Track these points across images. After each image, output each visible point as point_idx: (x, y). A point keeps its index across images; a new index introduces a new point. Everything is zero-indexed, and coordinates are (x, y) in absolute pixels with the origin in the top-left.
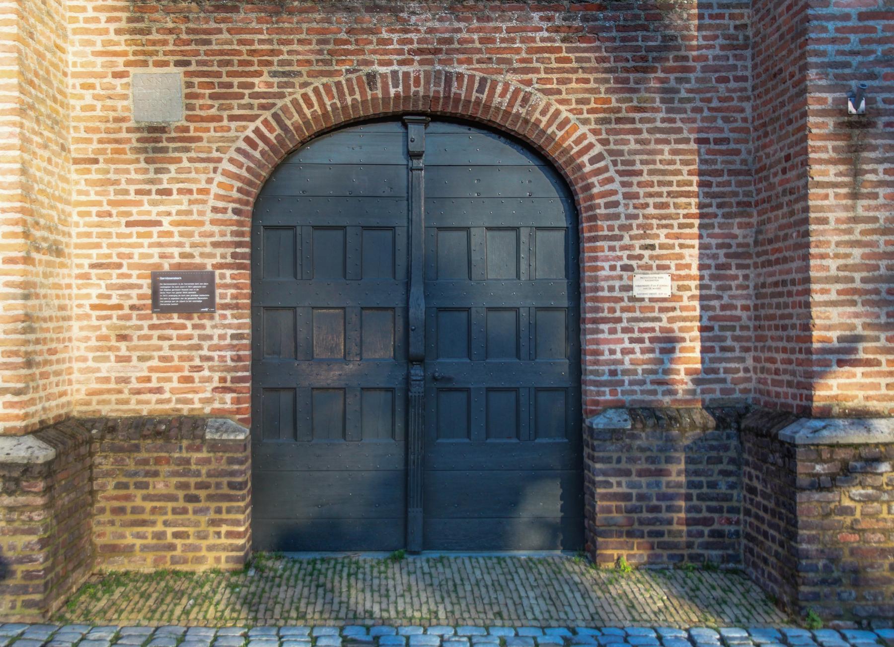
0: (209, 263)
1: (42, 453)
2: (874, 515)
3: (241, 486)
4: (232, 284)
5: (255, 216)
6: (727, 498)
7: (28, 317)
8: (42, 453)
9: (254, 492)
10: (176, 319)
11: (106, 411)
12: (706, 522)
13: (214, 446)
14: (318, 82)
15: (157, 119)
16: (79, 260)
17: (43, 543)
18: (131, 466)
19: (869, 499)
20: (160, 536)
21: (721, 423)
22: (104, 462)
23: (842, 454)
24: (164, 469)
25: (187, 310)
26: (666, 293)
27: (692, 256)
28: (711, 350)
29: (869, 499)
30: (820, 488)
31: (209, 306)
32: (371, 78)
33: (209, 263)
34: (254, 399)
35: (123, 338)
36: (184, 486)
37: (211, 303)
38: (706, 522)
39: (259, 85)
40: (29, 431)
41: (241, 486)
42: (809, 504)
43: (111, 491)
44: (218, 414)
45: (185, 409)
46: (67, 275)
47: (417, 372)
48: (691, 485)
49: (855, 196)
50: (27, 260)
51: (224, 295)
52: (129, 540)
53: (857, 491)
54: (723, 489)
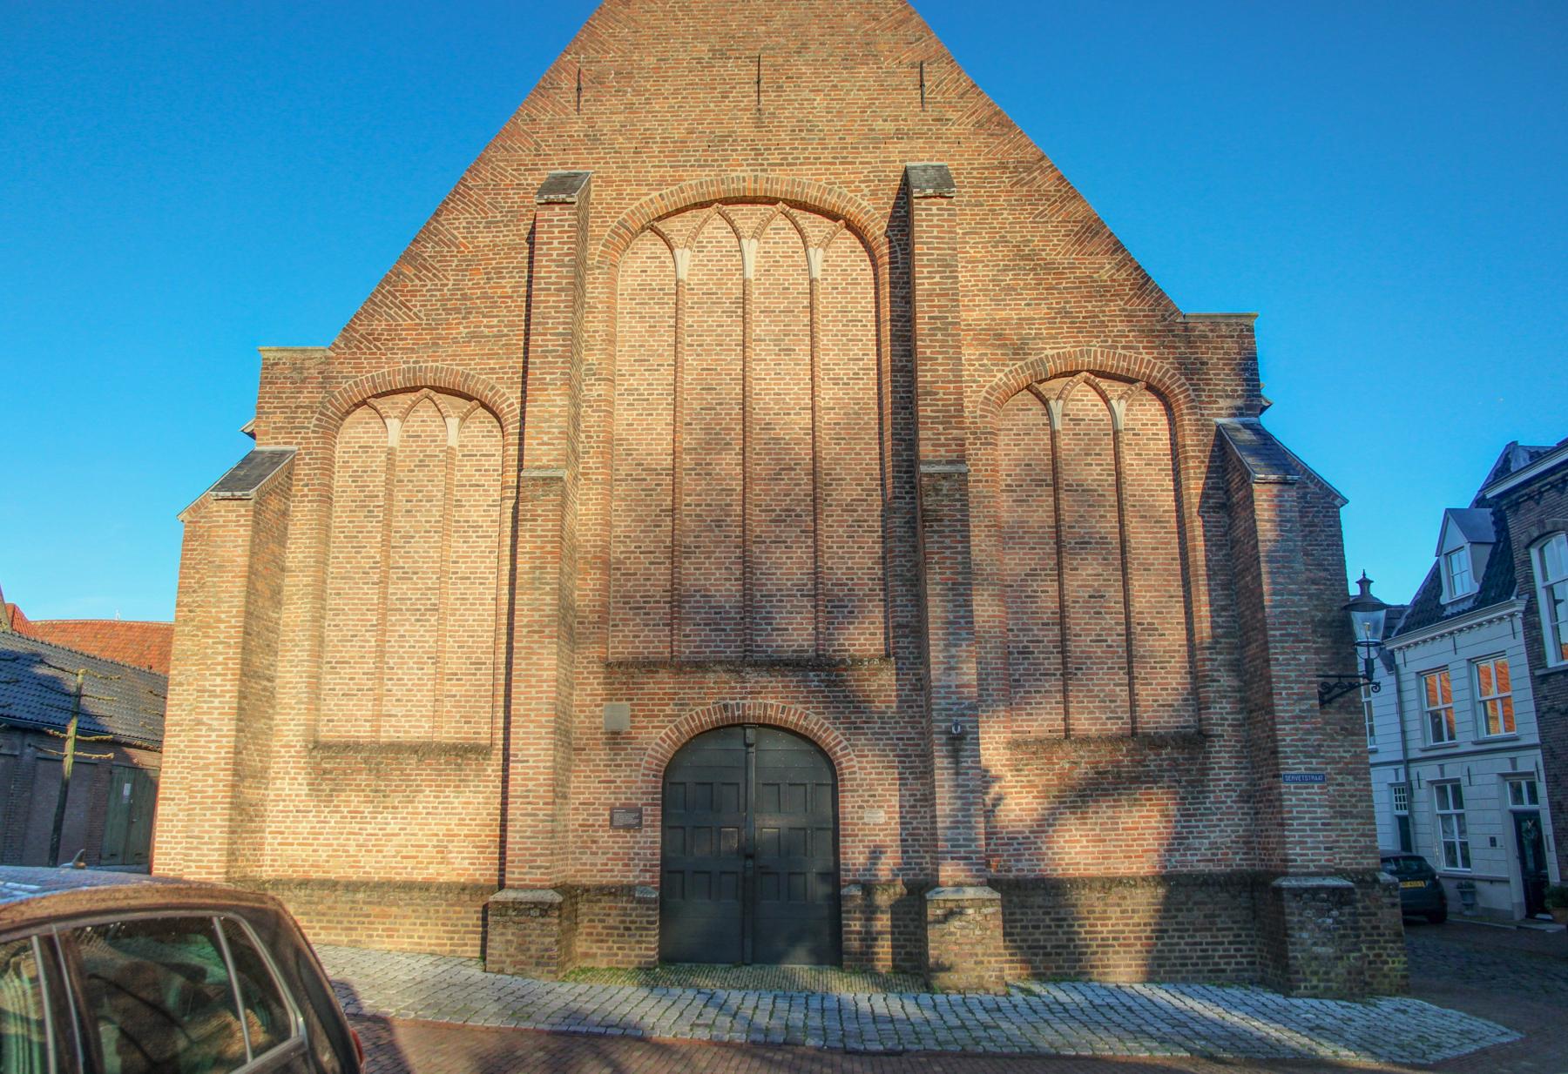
0: (640, 803)
1: (558, 898)
2: (966, 936)
3: (653, 923)
4: (653, 815)
5: (664, 778)
6: (914, 934)
7: (553, 831)
8: (558, 898)
9: (661, 927)
10: (622, 832)
11: (585, 881)
12: (903, 947)
13: (640, 901)
14: (699, 709)
15: (615, 728)
16: (575, 802)
17: (557, 942)
18: (597, 910)
19: (963, 928)
20: (610, 948)
21: (910, 892)
22: (583, 908)
23: (949, 905)
24: (614, 912)
25: (628, 828)
26: (882, 821)
27: (895, 801)
28: (233, 832)
29: (963, 928)
30: (939, 922)
31: (638, 826)
32: (726, 706)
33: (640, 803)
34: (662, 876)
35: (594, 842)
36: (623, 922)
37: (640, 824)
38: (903, 947)
39: (668, 710)
40: (555, 888)
41: (653, 923)
42: (933, 933)
43: (586, 923)
44: (643, 884)
45: (625, 881)
46: (568, 809)
47: (750, 863)
48: (893, 926)
49: (957, 774)
50: (554, 803)
51: (647, 820)
52: (594, 950)
53: (957, 923)
54: (912, 929)
